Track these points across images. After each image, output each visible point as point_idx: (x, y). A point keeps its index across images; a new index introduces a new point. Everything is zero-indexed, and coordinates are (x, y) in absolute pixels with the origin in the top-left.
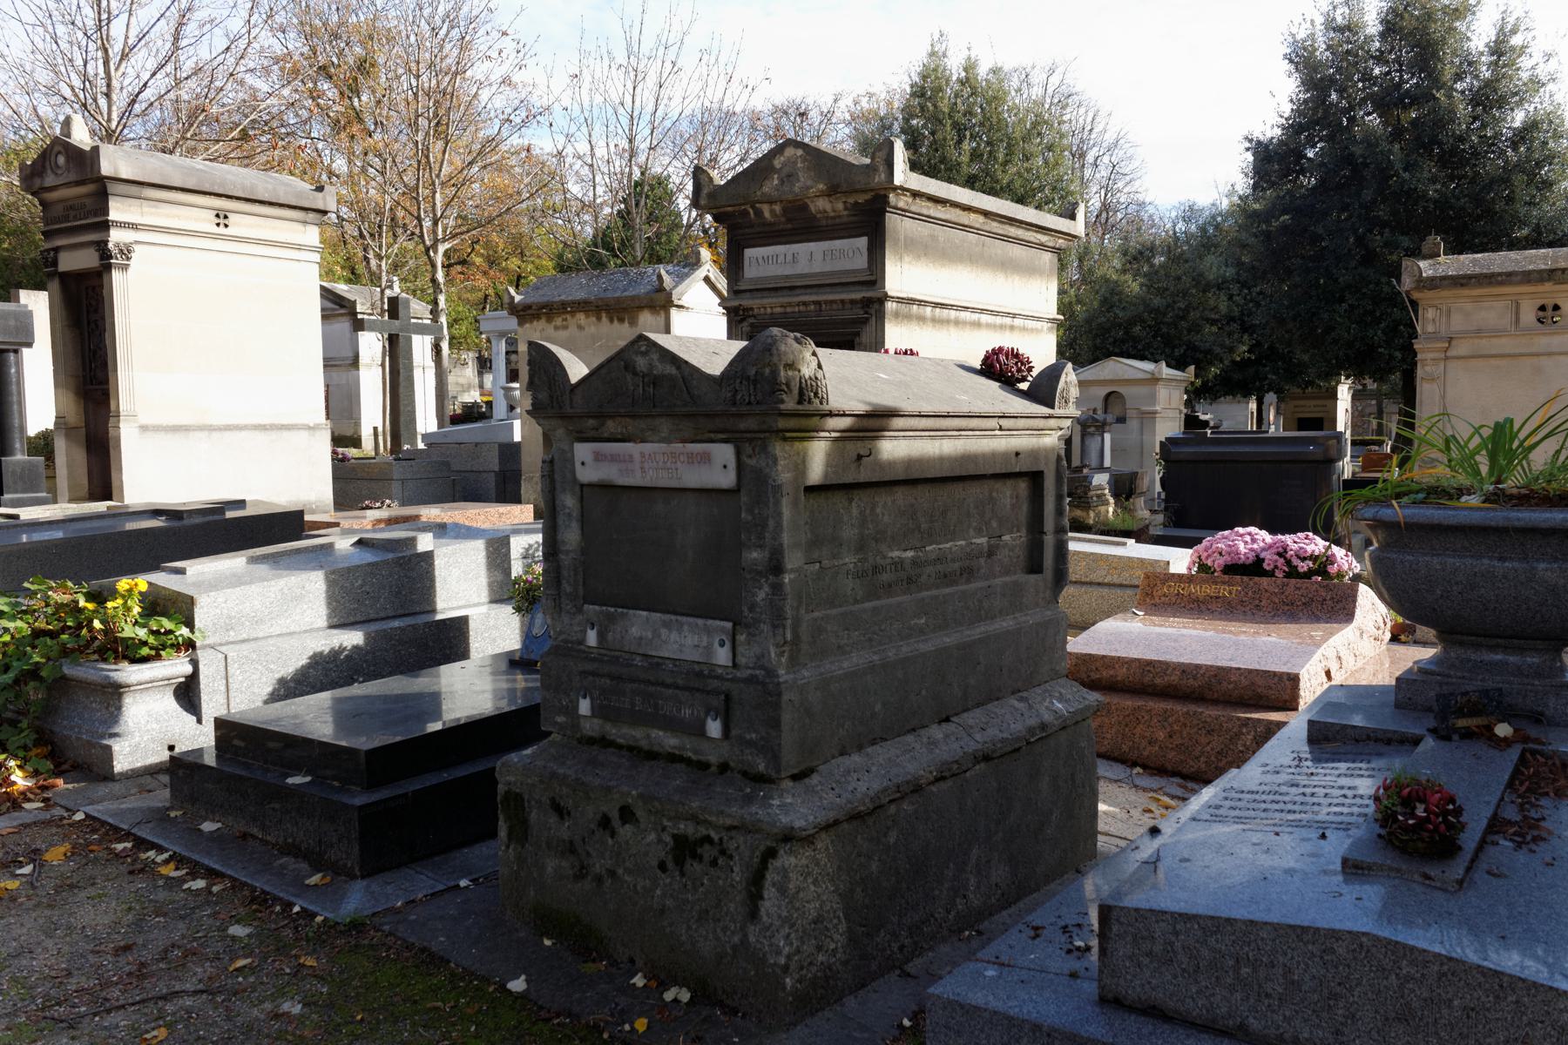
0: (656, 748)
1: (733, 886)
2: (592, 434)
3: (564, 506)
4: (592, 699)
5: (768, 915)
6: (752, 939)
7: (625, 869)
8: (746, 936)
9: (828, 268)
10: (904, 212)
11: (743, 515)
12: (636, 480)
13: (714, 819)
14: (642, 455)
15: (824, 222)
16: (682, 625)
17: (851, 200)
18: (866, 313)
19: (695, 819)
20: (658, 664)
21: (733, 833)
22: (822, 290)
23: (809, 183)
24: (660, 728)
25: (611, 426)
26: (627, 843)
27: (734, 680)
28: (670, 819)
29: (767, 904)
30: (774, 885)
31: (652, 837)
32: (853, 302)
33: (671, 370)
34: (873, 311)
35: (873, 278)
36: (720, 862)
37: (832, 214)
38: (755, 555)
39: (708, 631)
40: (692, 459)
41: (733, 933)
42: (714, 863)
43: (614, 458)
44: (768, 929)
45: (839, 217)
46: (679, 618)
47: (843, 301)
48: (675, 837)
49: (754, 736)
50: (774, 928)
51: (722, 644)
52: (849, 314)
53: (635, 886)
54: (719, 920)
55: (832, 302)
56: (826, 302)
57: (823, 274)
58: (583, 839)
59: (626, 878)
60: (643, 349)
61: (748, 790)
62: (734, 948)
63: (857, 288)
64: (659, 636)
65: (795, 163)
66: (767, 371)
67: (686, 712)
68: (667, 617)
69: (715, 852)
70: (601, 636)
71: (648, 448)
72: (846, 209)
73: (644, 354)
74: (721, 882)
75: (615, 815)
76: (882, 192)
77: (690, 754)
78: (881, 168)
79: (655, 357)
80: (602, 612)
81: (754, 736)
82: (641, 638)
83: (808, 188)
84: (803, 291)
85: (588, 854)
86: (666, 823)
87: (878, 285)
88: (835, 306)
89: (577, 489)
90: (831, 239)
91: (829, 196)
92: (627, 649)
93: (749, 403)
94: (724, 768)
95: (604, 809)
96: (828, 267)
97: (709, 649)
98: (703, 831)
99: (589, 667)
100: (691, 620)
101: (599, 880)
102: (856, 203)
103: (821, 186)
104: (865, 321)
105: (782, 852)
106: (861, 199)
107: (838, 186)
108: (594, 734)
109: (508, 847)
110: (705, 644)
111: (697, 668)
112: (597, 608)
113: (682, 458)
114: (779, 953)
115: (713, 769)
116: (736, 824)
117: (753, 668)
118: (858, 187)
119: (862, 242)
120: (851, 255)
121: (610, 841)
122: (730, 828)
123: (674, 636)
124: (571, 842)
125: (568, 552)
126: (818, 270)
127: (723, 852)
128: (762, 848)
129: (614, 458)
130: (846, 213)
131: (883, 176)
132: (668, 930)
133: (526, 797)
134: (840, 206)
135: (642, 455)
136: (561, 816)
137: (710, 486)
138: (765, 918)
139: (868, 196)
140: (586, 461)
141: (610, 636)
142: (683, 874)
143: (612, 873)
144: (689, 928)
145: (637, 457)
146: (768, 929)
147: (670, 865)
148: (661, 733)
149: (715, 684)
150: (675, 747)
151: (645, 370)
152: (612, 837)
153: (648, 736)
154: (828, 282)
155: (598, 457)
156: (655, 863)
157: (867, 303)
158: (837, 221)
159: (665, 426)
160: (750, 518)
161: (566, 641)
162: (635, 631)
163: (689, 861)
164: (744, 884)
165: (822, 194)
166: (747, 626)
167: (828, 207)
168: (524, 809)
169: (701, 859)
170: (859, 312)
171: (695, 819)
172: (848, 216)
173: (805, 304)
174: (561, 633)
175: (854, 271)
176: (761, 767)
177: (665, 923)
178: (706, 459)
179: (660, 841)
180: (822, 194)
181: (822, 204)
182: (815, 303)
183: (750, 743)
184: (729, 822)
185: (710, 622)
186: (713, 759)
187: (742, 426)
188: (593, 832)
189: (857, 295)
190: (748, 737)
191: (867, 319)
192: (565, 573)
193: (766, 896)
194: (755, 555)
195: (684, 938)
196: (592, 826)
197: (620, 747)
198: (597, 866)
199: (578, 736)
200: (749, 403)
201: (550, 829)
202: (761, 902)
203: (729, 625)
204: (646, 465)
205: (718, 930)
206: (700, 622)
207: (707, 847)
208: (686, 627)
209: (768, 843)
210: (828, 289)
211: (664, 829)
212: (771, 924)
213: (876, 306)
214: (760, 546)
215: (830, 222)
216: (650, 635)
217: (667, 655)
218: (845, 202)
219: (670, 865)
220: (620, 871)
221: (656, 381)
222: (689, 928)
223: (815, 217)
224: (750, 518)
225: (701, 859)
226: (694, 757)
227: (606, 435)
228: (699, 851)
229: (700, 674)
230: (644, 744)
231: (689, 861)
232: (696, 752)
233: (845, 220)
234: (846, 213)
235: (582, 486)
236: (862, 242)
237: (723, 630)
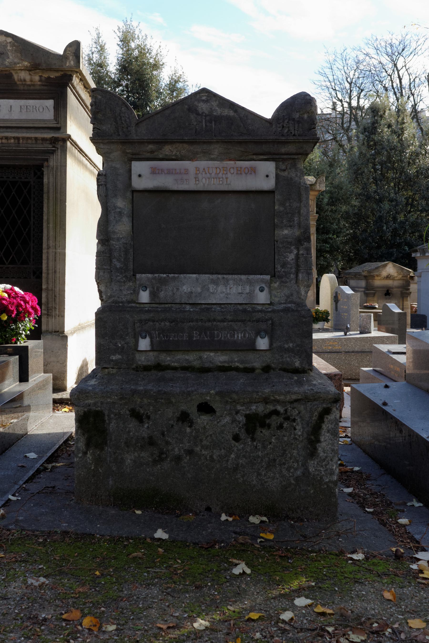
0: (207, 365)
1: (296, 439)
2: (148, 155)
3: (115, 207)
4: (151, 338)
5: (324, 452)
6: (311, 469)
7: (202, 447)
8: (307, 469)
9: (24, 117)
10: (70, 88)
11: (276, 207)
12: (191, 186)
13: (282, 397)
14: (197, 169)
15: (22, 88)
16: (228, 280)
17: (46, 75)
18: (54, 147)
19: (266, 401)
20: (208, 309)
21: (295, 405)
22: (20, 130)
23: (16, 60)
24: (211, 351)
25: (167, 150)
26: (204, 428)
27: (274, 311)
28: (243, 404)
29: (323, 444)
30: (328, 431)
31: (227, 419)
32: (44, 139)
33: (227, 112)
34: (59, 146)
35: (58, 126)
36: (285, 425)
37: (29, 83)
38: (286, 232)
39: (251, 283)
40: (240, 171)
41: (296, 469)
42: (280, 427)
43: (170, 172)
44: (324, 460)
45: (34, 85)
46: (225, 276)
47: (36, 139)
48: (247, 416)
49: (291, 345)
50: (329, 458)
51: (262, 290)
52: (41, 147)
53: (211, 457)
54: (284, 464)
55: (28, 138)
56: (23, 138)
57: (21, 120)
58: (163, 434)
59: (203, 452)
60: (204, 98)
61: (296, 378)
62: (297, 479)
63: (46, 131)
64: (208, 289)
65: (6, 46)
66: (306, 116)
67: (239, 336)
68: (215, 276)
69: (280, 420)
70: (153, 295)
71: (203, 164)
72: (40, 81)
73: (206, 101)
74: (286, 439)
75: (193, 411)
76: (69, 73)
77: (237, 364)
78: (71, 58)
79: (214, 104)
80: (154, 278)
81: (291, 345)
82: (191, 293)
83: (15, 64)
84: (4, 130)
85: (167, 443)
86: (239, 407)
87: (62, 130)
88: (30, 141)
89: (129, 194)
90: (26, 99)
91: (30, 70)
92: (178, 301)
93: (294, 135)
94: (267, 369)
95: (183, 407)
96: (24, 117)
97: (251, 294)
98: (271, 407)
99: (144, 317)
100: (236, 276)
101: (178, 459)
102: (49, 78)
103: (26, 63)
104: (53, 152)
105: (334, 409)
106: (53, 75)
107: (39, 65)
108: (149, 363)
109: (85, 453)
110: (248, 291)
111: (240, 308)
112: (150, 276)
113: (232, 171)
114: (332, 473)
115: (257, 371)
116: (300, 398)
117: (285, 303)
118: (54, 67)
119: (50, 103)
120: (41, 110)
121: (188, 430)
122: (291, 402)
123: (221, 288)
124: (150, 438)
125: (118, 239)
126: (16, 118)
127: (287, 419)
128: (320, 409)
129: (170, 172)
130: (39, 83)
131: (72, 63)
132: (241, 480)
133: (106, 413)
134: (37, 78)
135: (197, 169)
136: (141, 421)
137: (254, 189)
138: (322, 454)
139: (58, 74)
140: (142, 173)
141: (162, 294)
142: (253, 439)
143: (190, 452)
144: (259, 474)
145: (192, 171)
146: (324, 460)
147: (243, 435)
148: (212, 354)
149: (260, 315)
150: (225, 362)
151: (207, 113)
152: (190, 427)
153: (201, 358)
154: (25, 125)
155: (154, 171)
156: (230, 437)
157: (54, 141)
158: (32, 88)
159: (216, 149)
160: (282, 209)
161: (116, 302)
162: (186, 289)
163: (259, 429)
164: (305, 435)
165: (26, 69)
166: (280, 277)
167: (28, 78)
168: (104, 421)
169: (269, 426)
170: (50, 147)
171: (266, 401)
172: (40, 85)
173: (7, 138)
174: (110, 297)
175: (44, 121)
176: (297, 364)
177: (239, 476)
178: (253, 171)
179: (234, 421)
180: (26, 69)
181: (24, 75)
182: (14, 138)
183: (288, 350)
184: (294, 397)
185: (251, 277)
186: (257, 365)
187: (283, 150)
188: (172, 426)
189: (48, 135)
190: (286, 346)
191: (54, 151)
192: (116, 254)
193: (322, 440)
194: (286, 232)
195: (255, 482)
196: (171, 422)
197: (175, 369)
198: (176, 449)
199: (134, 366)
200: (294, 135)
201: (129, 432)
202: (318, 445)
203: (268, 277)
204: (200, 176)
205: (284, 471)
206: (243, 277)
207: (274, 417)
208: (231, 282)
209: (325, 406)
210: (24, 130)
211: (237, 412)
212: (326, 457)
213: (61, 143)
214: (291, 226)
215: (26, 88)
216: (199, 290)
217: (214, 302)
218: (41, 76)
219: (243, 435)
220: (198, 449)
221: (218, 119)
222: (259, 474)
223: (16, 83)
224: (282, 209)
225: (269, 426)
226: (241, 366)
227: (161, 156)
228: (268, 421)
229: (245, 311)
230: (196, 364)
231: (259, 429)
232: (242, 362)
233: (38, 88)
234: (39, 83)
235: (134, 191)
236: (50, 103)
237: (262, 281)
